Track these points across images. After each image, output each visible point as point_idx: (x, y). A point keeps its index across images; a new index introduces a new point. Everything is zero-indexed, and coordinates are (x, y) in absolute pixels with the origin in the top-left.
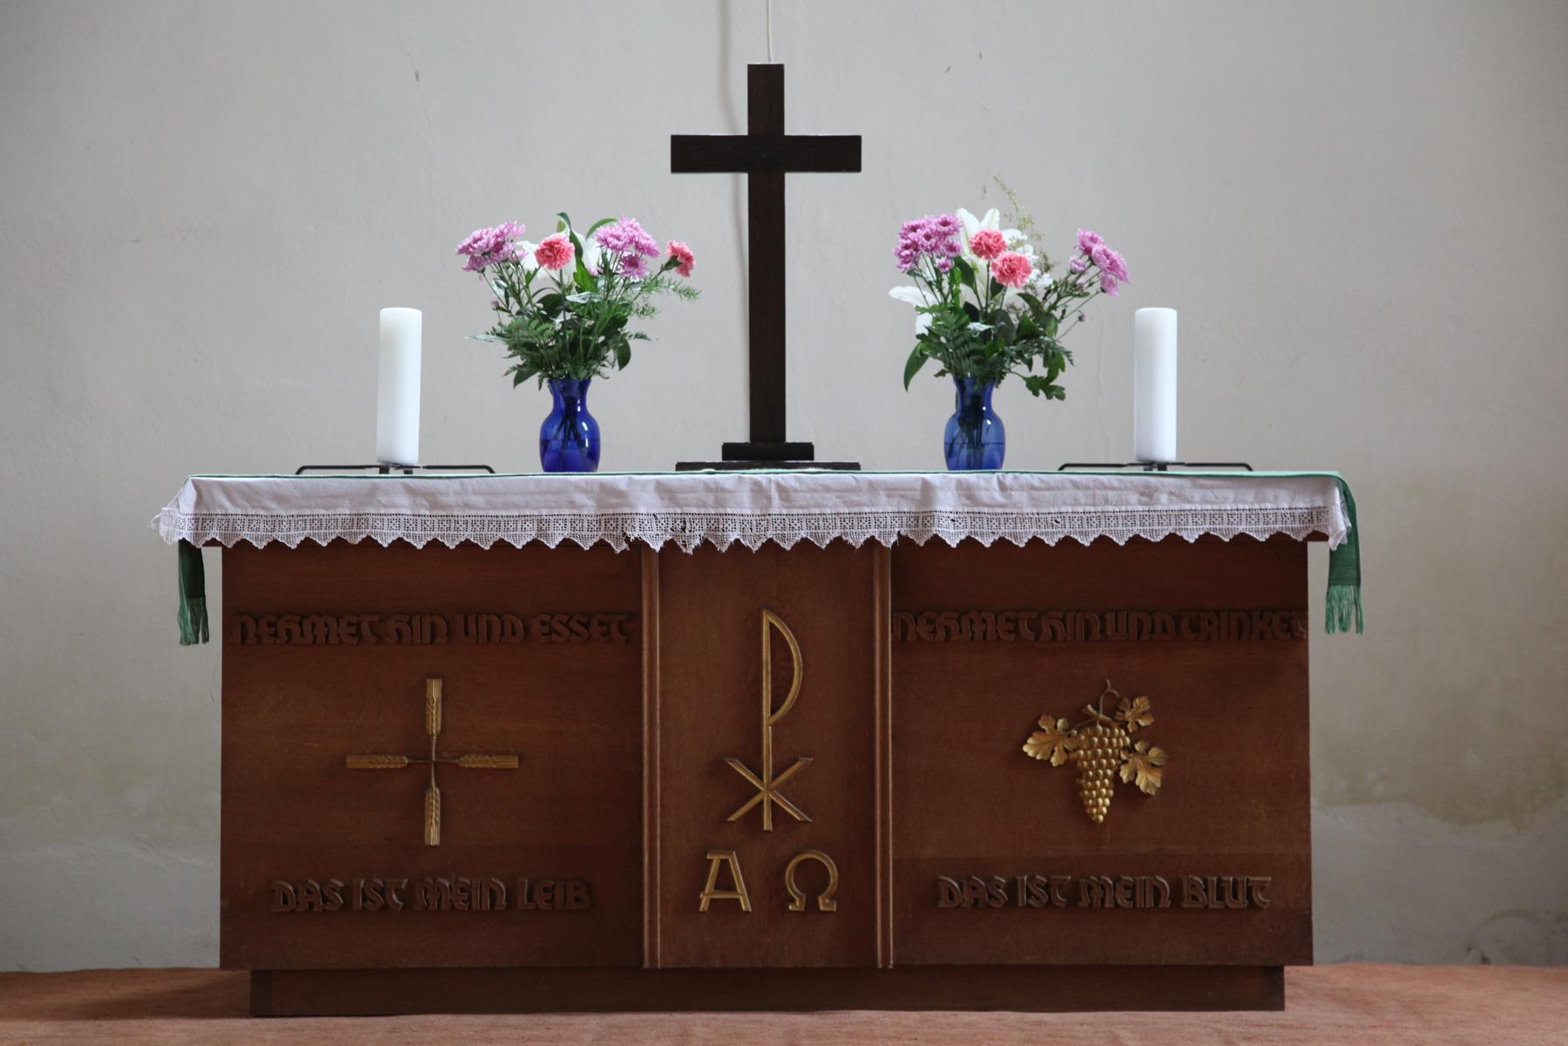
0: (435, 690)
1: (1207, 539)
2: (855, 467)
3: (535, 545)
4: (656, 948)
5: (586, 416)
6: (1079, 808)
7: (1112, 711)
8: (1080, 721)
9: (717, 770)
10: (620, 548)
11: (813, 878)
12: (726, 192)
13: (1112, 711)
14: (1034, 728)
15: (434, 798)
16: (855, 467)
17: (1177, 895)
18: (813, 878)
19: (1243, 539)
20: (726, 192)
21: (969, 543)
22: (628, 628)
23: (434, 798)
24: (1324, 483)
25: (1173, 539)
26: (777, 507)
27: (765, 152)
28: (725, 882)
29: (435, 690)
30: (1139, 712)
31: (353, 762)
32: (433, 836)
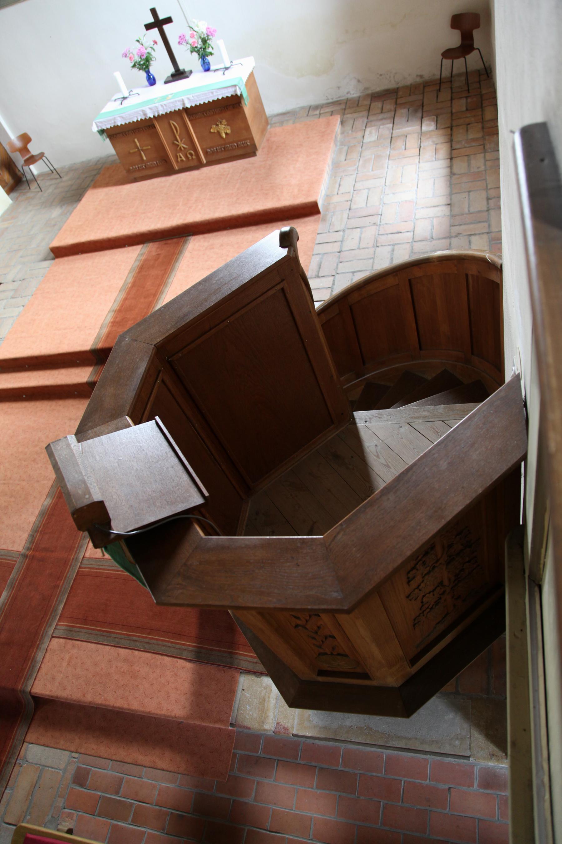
0: (136, 140)
1: (223, 98)
2: (59, 253)
3: (137, 121)
4: (177, 168)
5: (152, 75)
6: (221, 137)
7: (221, 123)
8: (217, 125)
9: (174, 144)
10: (148, 118)
11: (191, 154)
12: (155, 31)
13: (221, 123)
14: (211, 128)
15: (142, 153)
16: (59, 253)
17: (238, 146)
18: (191, 154)
19: (227, 97)
20: (155, 31)
21: (191, 106)
22: (154, 127)
23: (142, 153)
24: (235, 86)
25: (218, 99)
26: (165, 107)
27: (158, 23)
28: (181, 157)
29: (136, 140)
30: (224, 122)
31: (131, 151)
32: (145, 158)
